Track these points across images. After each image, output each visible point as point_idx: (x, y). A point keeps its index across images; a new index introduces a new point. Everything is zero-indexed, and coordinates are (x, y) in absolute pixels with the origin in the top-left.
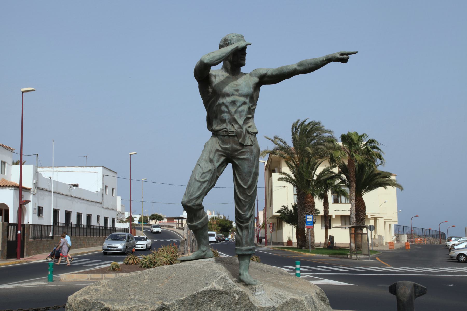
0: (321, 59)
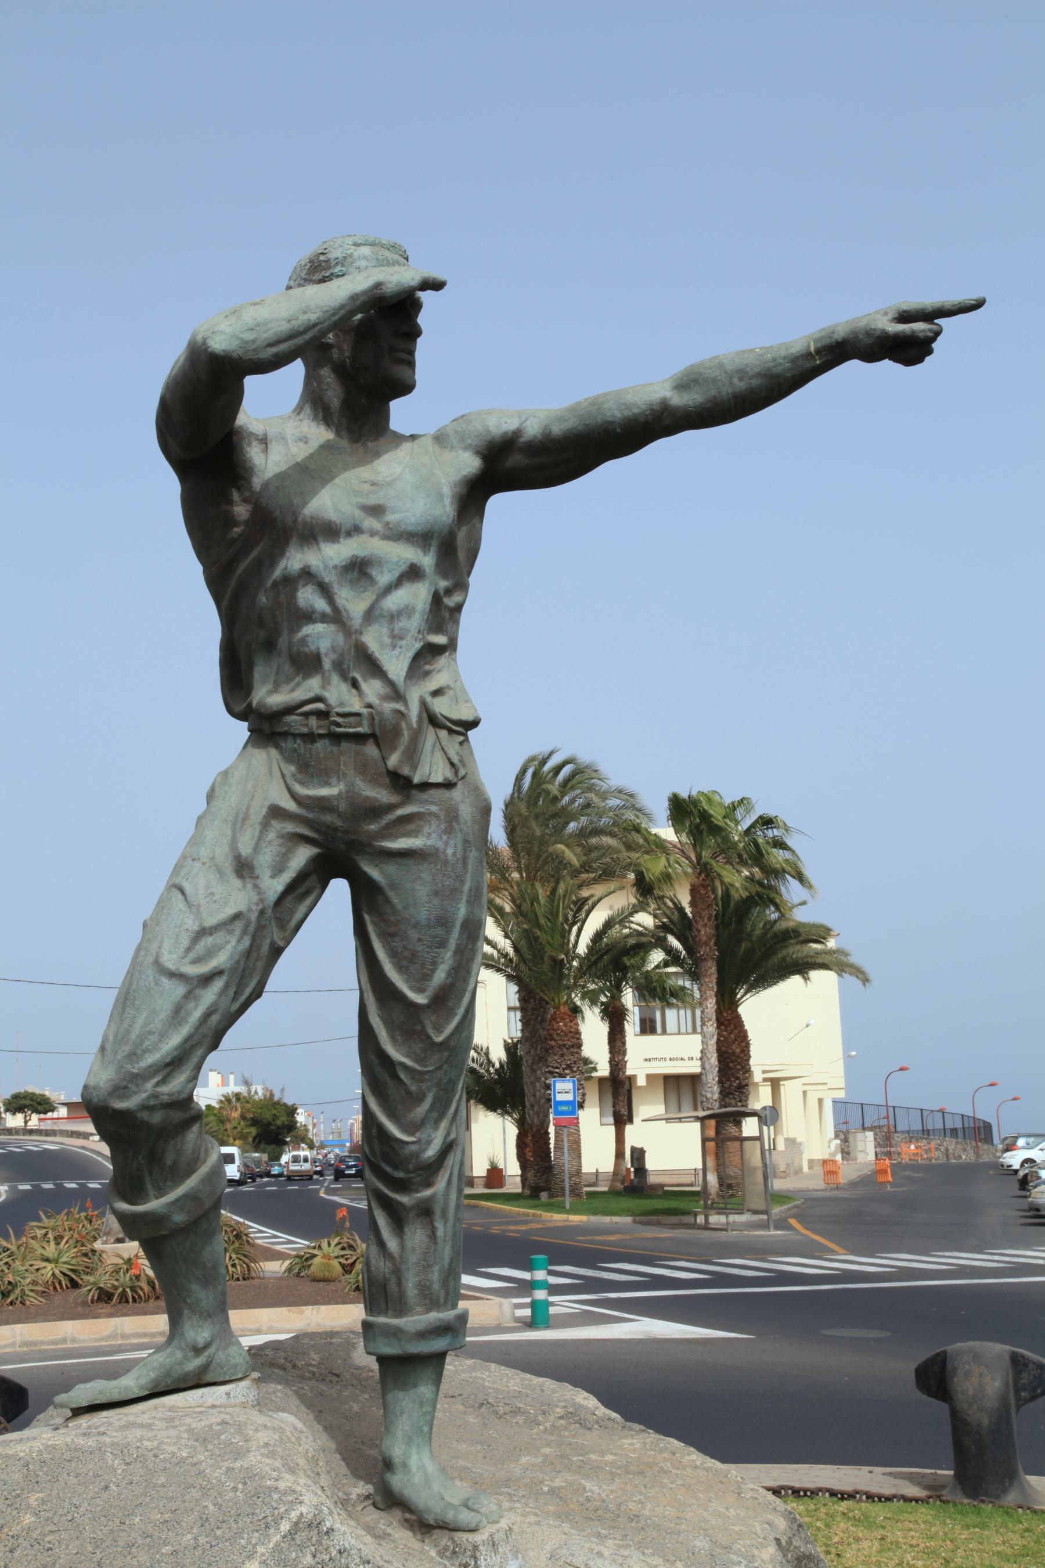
0: (797, 348)
